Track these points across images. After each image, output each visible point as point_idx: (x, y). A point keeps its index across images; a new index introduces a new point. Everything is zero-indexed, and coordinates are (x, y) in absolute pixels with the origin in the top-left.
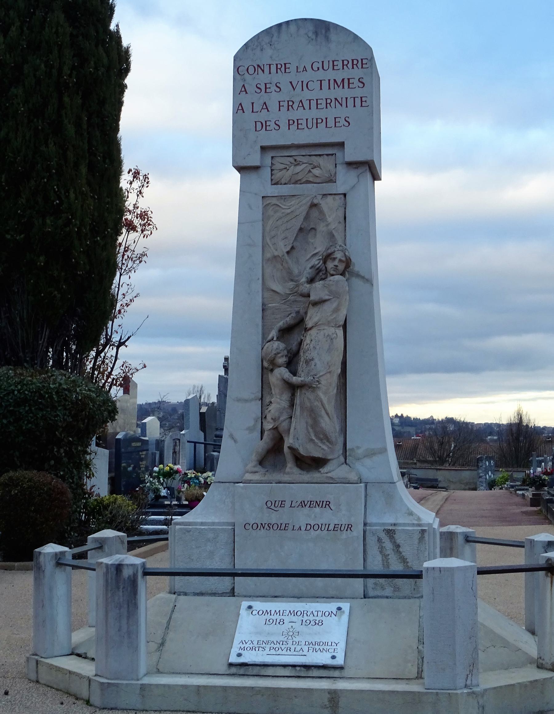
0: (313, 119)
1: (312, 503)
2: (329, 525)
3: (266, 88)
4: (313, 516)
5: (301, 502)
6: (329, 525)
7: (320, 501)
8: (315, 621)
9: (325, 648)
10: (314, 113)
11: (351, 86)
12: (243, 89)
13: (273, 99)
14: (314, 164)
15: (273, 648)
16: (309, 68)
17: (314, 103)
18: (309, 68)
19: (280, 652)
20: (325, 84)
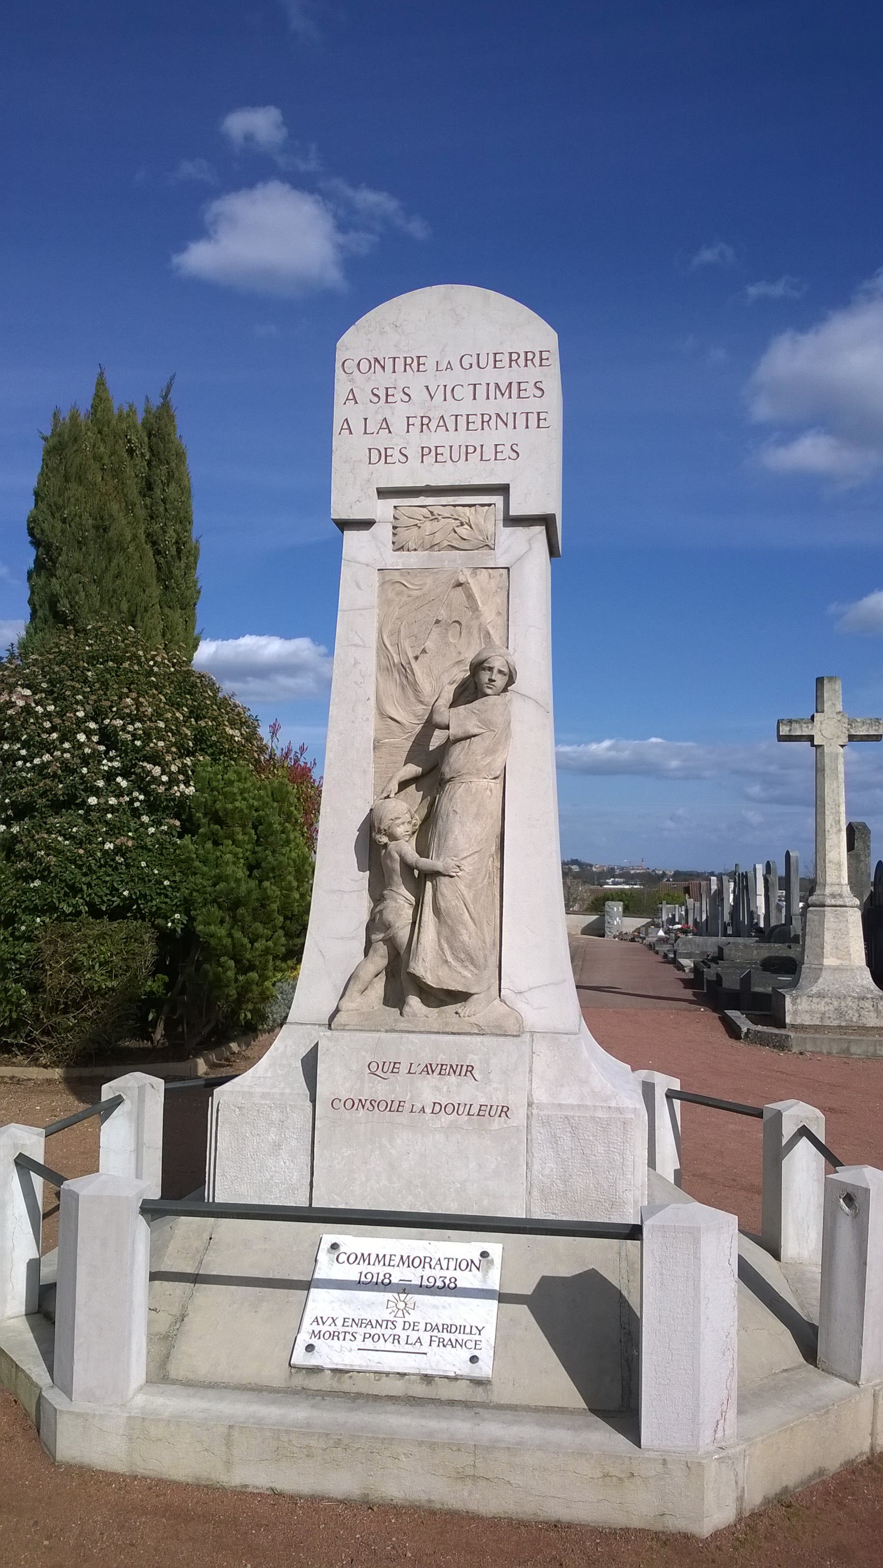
0: (460, 446)
1: (444, 1067)
2: (471, 1105)
3: (387, 395)
4: (445, 1089)
5: (426, 1066)
6: (471, 1105)
7: (457, 1065)
8: (442, 1279)
9: (461, 1337)
10: (461, 438)
11: (522, 394)
12: (351, 397)
13: (398, 414)
14: (460, 519)
15: (370, 1335)
16: (456, 364)
17: (462, 421)
18: (456, 364)
19: (381, 1345)
20: (481, 391)
